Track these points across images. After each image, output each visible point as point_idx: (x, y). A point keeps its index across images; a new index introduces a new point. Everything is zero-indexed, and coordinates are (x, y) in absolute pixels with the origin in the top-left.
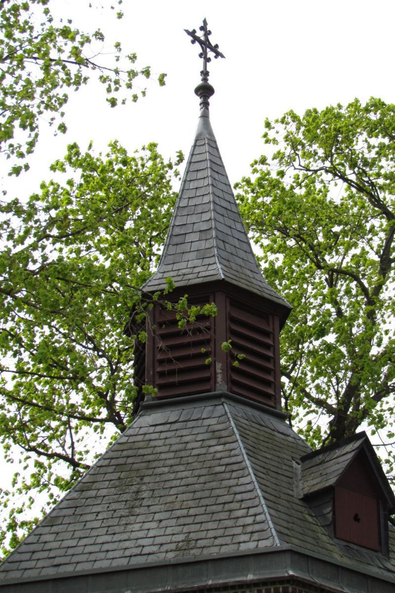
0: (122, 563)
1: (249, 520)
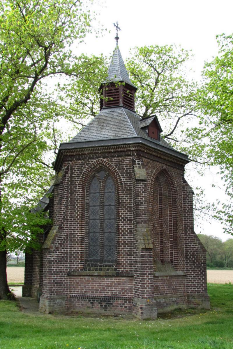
0: (101, 139)
1: (130, 131)
